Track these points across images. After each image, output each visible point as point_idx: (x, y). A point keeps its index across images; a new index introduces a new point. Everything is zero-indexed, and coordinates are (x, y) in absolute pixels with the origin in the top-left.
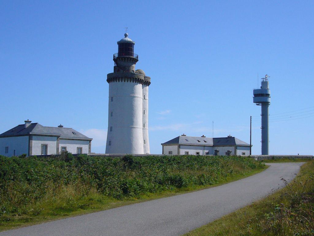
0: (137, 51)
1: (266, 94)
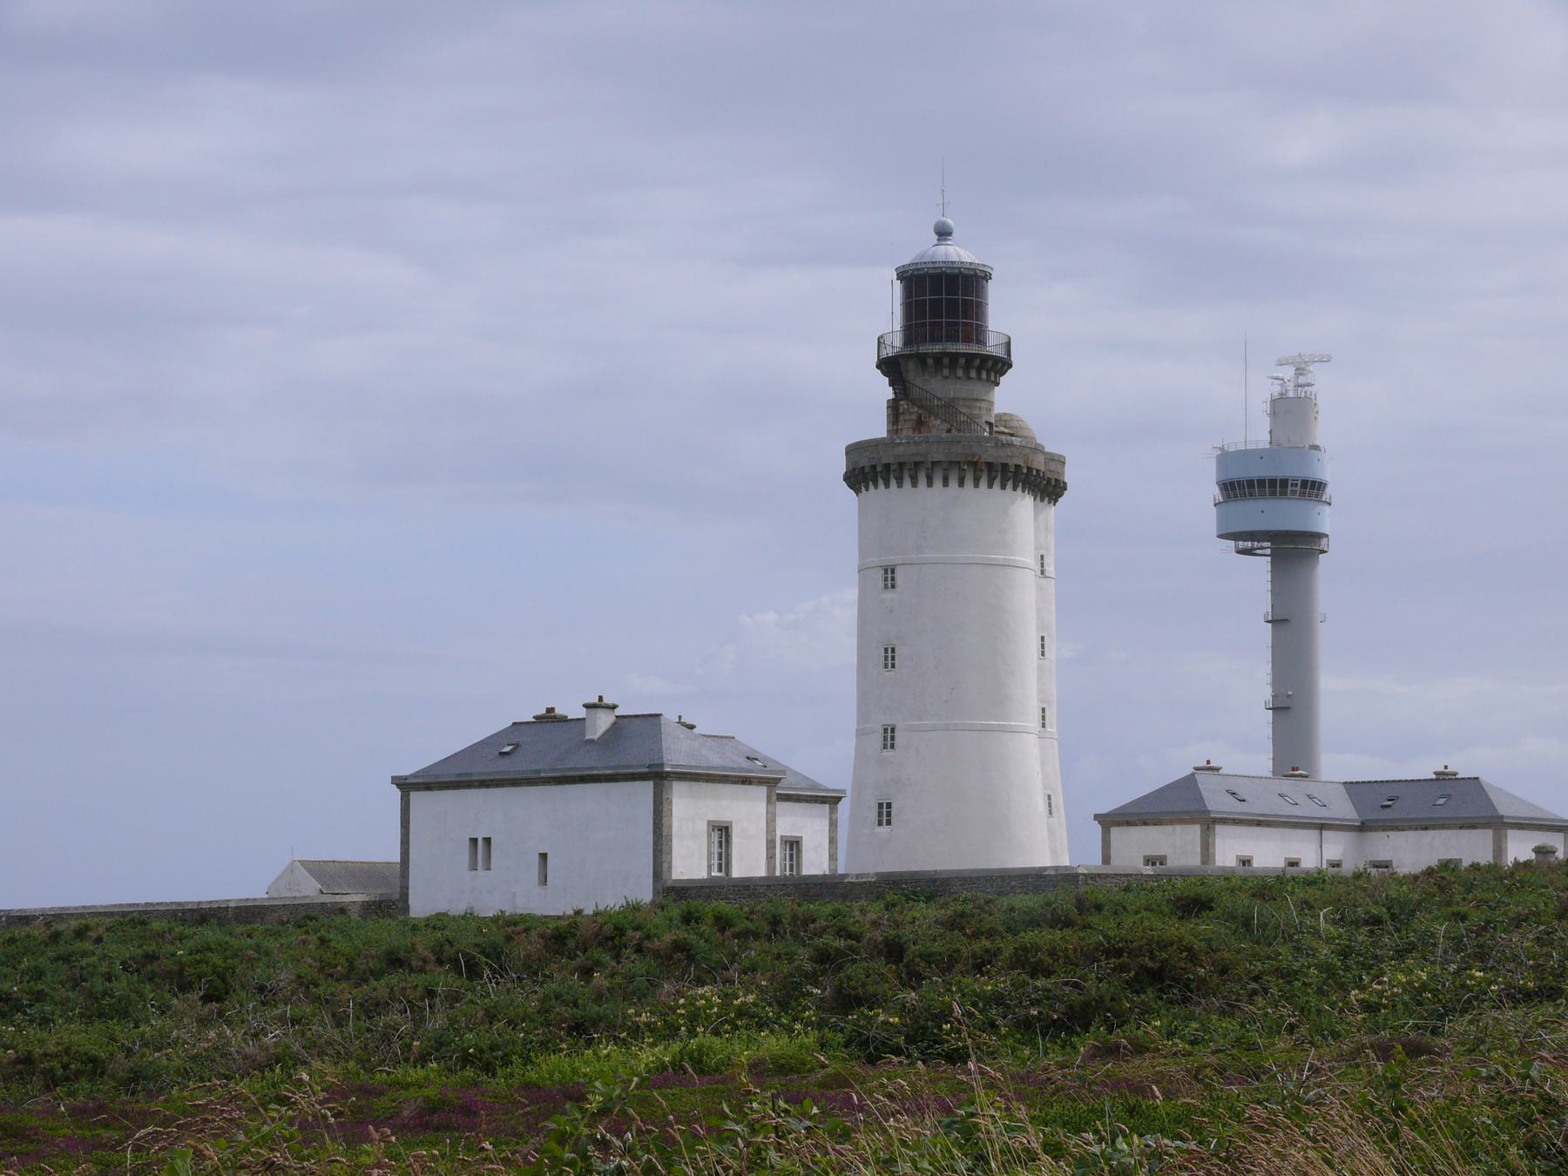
0: (1004, 316)
1: (1305, 483)
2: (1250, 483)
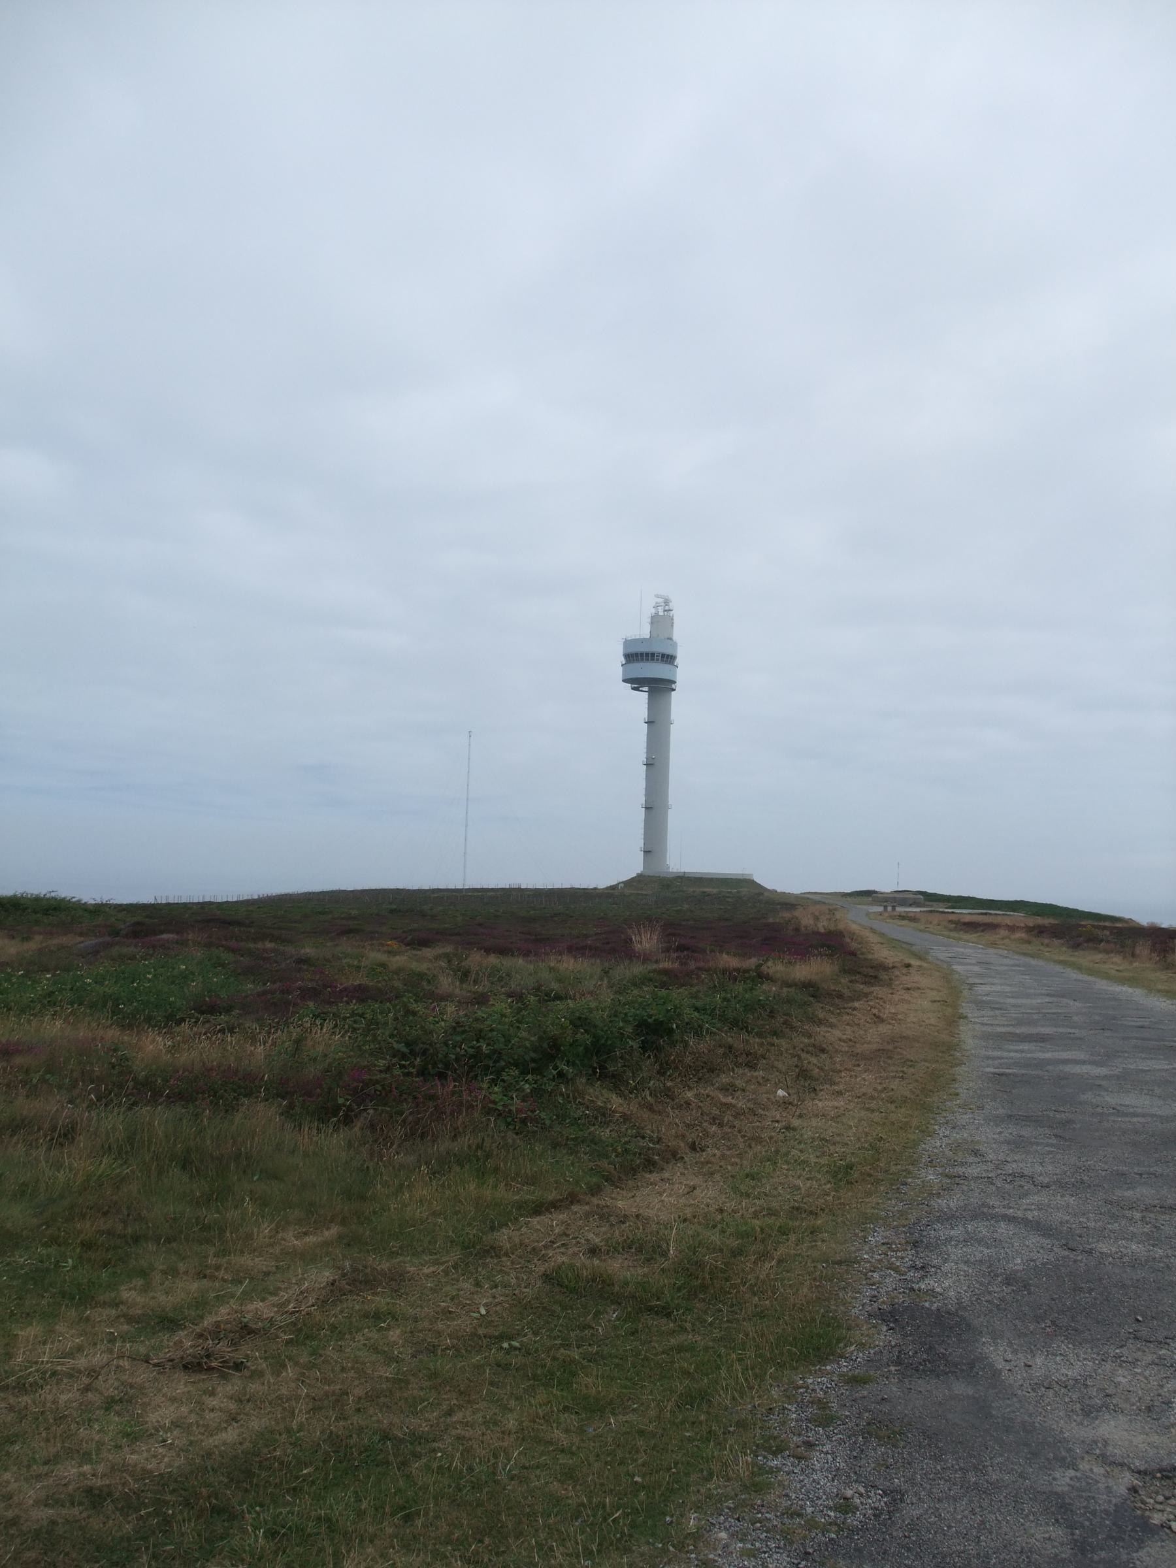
2: (637, 654)
